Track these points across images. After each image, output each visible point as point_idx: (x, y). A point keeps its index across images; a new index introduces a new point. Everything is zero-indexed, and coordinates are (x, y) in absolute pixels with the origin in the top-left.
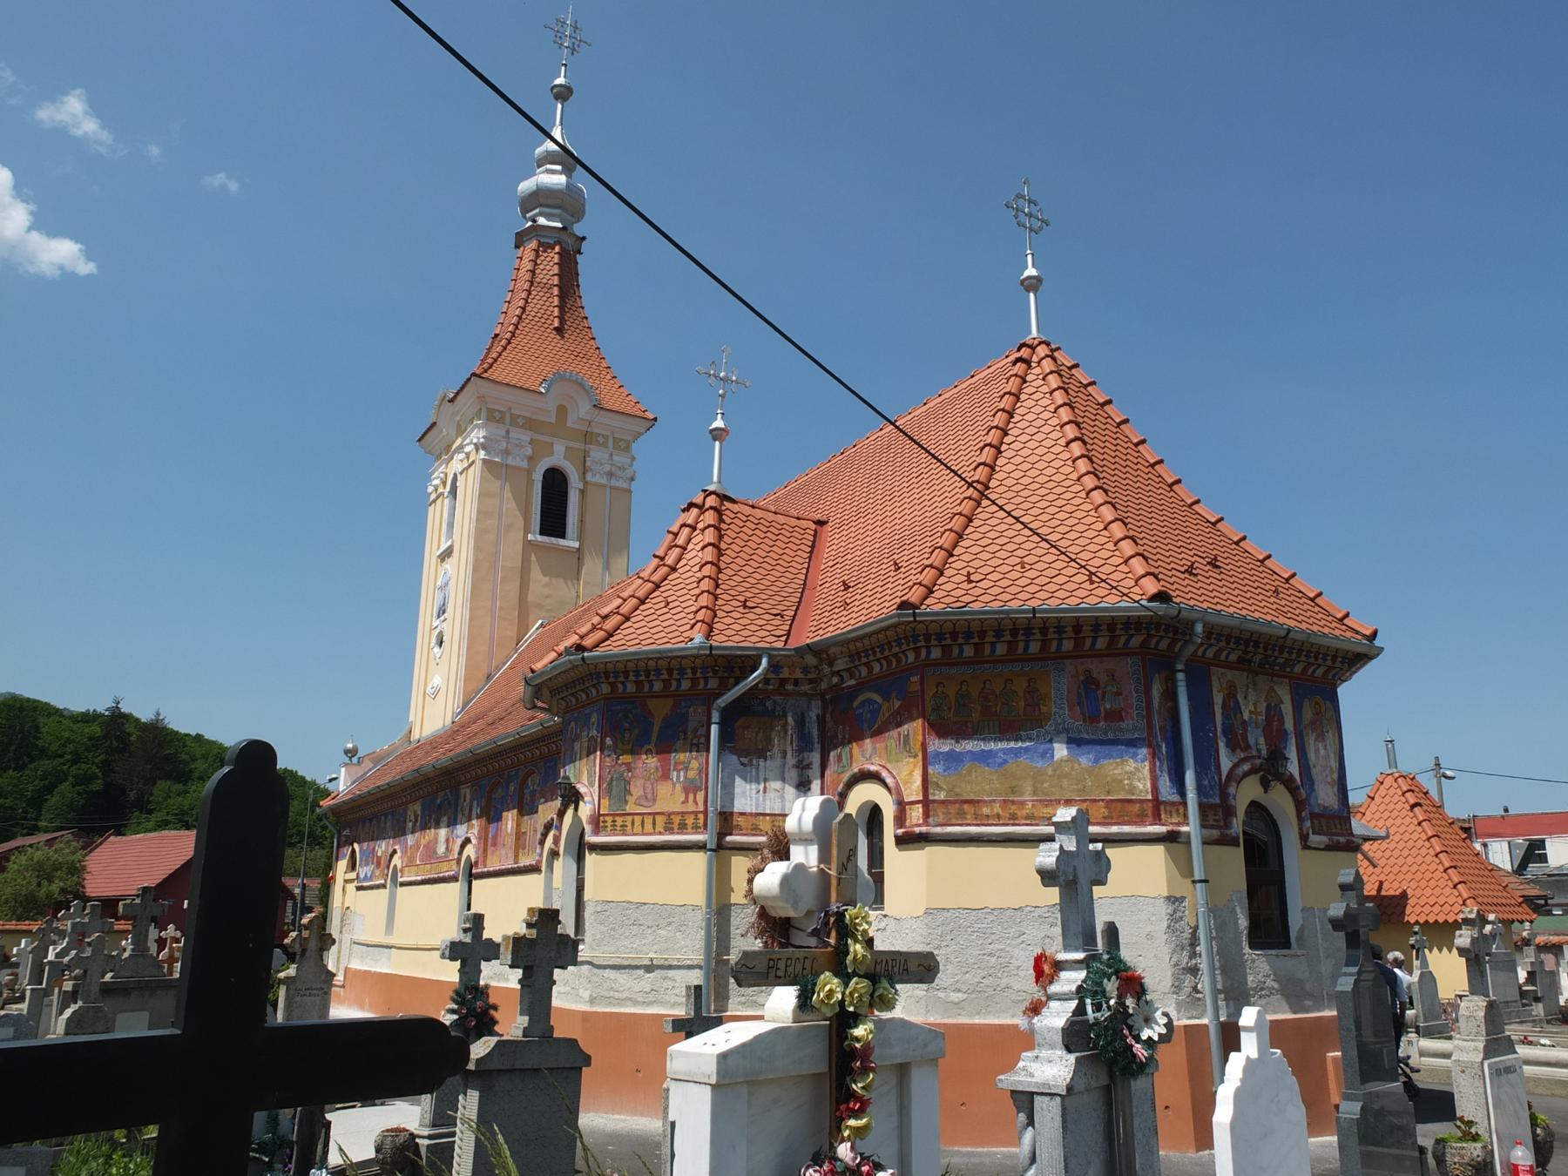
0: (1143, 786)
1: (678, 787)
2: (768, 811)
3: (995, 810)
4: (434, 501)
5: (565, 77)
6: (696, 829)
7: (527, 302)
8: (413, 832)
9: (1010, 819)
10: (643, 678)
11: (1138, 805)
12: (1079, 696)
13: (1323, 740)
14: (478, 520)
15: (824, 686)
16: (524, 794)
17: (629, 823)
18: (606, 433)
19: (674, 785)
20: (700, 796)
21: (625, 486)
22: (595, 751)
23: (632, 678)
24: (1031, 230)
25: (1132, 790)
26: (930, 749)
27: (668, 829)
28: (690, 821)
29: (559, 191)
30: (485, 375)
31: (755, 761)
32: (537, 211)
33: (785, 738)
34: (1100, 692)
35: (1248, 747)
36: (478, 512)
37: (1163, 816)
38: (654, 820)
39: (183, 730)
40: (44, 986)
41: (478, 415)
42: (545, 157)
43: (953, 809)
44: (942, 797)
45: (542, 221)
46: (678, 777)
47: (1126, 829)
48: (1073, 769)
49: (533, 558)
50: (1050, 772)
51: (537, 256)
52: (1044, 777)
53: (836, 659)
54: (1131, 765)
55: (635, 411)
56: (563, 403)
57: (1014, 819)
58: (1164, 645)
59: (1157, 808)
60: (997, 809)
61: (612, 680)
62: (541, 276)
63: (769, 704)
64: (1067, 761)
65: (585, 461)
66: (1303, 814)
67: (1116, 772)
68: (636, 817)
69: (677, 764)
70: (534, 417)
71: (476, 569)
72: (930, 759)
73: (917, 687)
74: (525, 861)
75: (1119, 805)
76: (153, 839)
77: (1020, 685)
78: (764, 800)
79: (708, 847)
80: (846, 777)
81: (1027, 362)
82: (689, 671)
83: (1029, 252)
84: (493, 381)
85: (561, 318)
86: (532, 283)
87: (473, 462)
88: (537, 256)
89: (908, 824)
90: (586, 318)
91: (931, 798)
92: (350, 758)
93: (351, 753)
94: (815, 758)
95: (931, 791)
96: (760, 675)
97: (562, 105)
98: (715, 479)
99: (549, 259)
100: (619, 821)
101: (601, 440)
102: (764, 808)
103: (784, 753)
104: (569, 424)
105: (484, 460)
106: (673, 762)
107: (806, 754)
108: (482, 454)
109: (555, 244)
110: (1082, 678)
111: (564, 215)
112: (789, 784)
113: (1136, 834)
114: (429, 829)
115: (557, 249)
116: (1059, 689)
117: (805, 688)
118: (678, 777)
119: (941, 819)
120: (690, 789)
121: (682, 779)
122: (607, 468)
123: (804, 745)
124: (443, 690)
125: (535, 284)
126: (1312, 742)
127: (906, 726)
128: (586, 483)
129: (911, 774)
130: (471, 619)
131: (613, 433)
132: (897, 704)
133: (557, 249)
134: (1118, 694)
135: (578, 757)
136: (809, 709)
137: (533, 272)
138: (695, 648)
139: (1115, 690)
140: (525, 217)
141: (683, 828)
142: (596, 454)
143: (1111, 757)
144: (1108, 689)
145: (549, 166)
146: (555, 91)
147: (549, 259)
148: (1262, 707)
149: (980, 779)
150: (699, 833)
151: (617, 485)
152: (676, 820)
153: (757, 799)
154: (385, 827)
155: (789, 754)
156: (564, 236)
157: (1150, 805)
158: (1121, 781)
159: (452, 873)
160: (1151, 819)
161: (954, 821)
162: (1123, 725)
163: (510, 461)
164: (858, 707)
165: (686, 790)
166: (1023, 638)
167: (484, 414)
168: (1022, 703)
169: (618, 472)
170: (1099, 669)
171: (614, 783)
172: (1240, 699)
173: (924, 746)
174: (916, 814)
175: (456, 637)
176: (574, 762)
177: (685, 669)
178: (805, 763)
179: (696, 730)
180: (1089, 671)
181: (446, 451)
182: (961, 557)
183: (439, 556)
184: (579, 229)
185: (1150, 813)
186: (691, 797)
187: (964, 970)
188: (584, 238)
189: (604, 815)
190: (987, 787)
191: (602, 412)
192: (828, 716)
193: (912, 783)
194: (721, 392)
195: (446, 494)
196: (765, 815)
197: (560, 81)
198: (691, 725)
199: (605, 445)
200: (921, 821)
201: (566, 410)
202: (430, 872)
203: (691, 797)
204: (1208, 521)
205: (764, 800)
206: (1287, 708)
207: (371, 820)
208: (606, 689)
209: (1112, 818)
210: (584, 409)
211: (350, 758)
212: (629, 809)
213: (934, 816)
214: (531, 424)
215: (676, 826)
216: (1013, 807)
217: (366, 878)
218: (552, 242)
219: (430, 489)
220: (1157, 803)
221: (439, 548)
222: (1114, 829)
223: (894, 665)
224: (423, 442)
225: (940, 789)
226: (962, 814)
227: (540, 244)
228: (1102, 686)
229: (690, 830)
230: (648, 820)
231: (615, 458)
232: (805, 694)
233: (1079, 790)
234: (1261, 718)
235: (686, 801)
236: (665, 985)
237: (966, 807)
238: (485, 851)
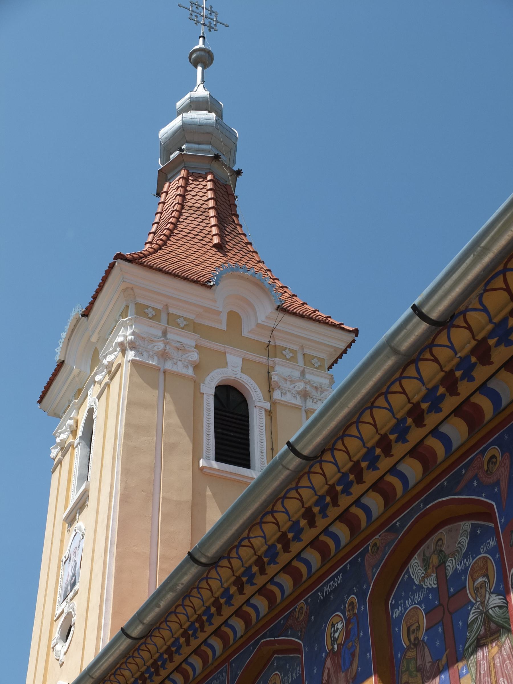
4: (60, 462)
14: (127, 435)
18: (295, 347)
36: (128, 424)
41: (124, 313)
49: (209, 492)
51: (187, 184)
71: (125, 499)
85: (221, 235)
97: (204, 68)
101: (289, 355)
104: (245, 333)
105: (133, 362)
108: (131, 355)
115: (209, 177)
122: (301, 386)
128: (274, 403)
130: (119, 570)
131: (302, 348)
137: (183, 196)
146: (194, 56)
147: (200, 187)
163: (169, 366)
167: (132, 309)
169: (314, 393)
183: (66, 519)
197: (200, 44)
199: (294, 359)
201: (239, 318)
231: (308, 377)
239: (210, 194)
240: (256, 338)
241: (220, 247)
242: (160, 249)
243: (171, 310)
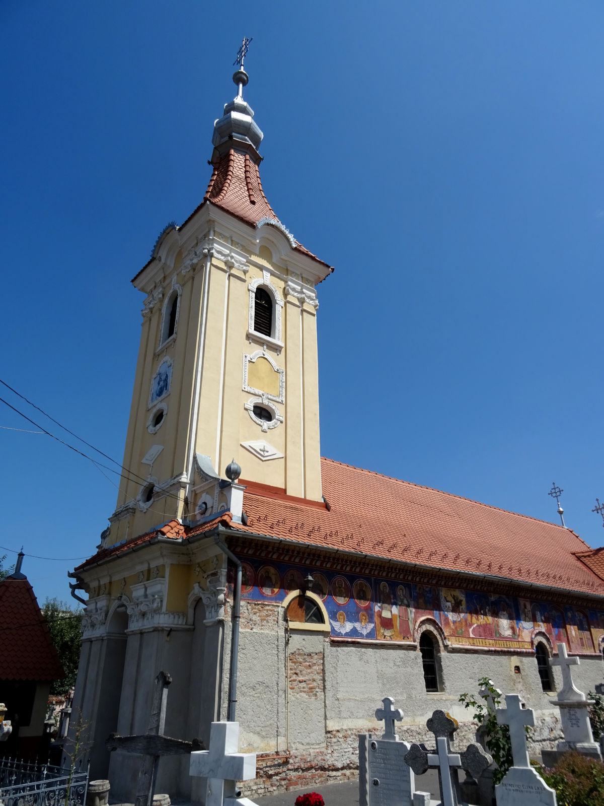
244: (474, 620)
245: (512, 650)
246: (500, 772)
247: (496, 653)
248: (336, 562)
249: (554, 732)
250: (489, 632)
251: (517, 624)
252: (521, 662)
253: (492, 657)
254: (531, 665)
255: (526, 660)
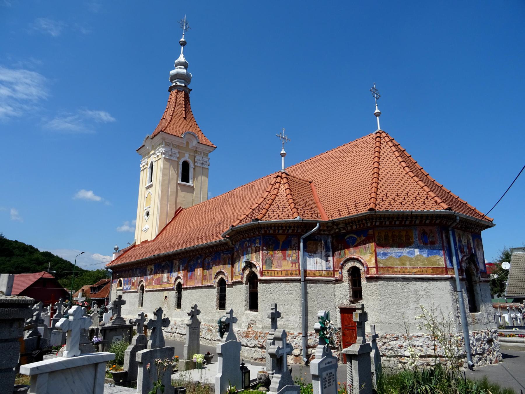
0: (442, 264)
1: (289, 262)
2: (318, 270)
3: (398, 270)
4: (143, 170)
5: (184, 38)
6: (296, 275)
7: (175, 109)
8: (150, 275)
9: (403, 272)
10: (277, 229)
11: (441, 269)
12: (422, 236)
13: (480, 251)
14: (163, 177)
15: (332, 232)
16: (204, 263)
17: (273, 273)
19: (288, 261)
20: (297, 265)
21: (207, 167)
22: (259, 251)
23: (273, 229)
24: (377, 98)
25: (439, 264)
26: (377, 252)
27: (287, 275)
28: (294, 273)
29: (184, 75)
30: (165, 131)
31: (313, 254)
32: (176, 80)
33: (321, 248)
34: (428, 236)
35: (464, 252)
36: (163, 174)
37: (448, 272)
38: (282, 272)
39: (10, 239)
40: (51, 327)
41: (161, 144)
42: (179, 64)
43: (385, 270)
44: (382, 266)
45: (178, 83)
46: (289, 259)
47: (439, 276)
48: (421, 258)
50: (414, 259)
51: (177, 94)
52: (412, 260)
53: (340, 224)
54: (438, 257)
55: (210, 144)
56: (188, 141)
57: (404, 273)
58: (444, 222)
59: (446, 270)
60: (399, 269)
61: (266, 229)
62: (179, 101)
63: (316, 237)
64: (419, 256)
65: (195, 159)
66: (478, 272)
67: (434, 259)
68: (275, 271)
69: (288, 255)
70: (179, 145)
72: (378, 254)
73: (372, 233)
74: (206, 284)
75: (435, 269)
76: (19, 276)
77: (404, 233)
78: (316, 266)
79: (301, 280)
80: (344, 260)
81: (380, 137)
82: (292, 227)
83: (376, 105)
84: (167, 133)
85: (186, 114)
86: (176, 103)
87: (160, 158)
88: (177, 94)
89: (370, 273)
90: (193, 115)
91: (378, 266)
92: (116, 251)
93: (116, 249)
94: (331, 253)
95: (378, 264)
96: (317, 229)
98: (283, 168)
99: (181, 96)
100: (270, 272)
102: (317, 269)
103: (322, 252)
104: (190, 148)
105: (164, 158)
106: (287, 255)
107: (328, 252)
108: (164, 156)
109: (183, 91)
110: (422, 231)
111: (185, 82)
112: (324, 260)
113: (442, 277)
114: (159, 273)
115: (183, 92)
116: (415, 235)
117: (327, 232)
118: (289, 259)
119: (382, 272)
120: (294, 263)
121: (290, 259)
122: (201, 162)
123: (327, 250)
124: (150, 229)
125: (177, 103)
126: (477, 251)
127: (368, 245)
128: (195, 166)
129: (370, 259)
131: (203, 151)
132: (363, 238)
133: (183, 92)
134: (433, 236)
135: (250, 252)
136: (328, 239)
137: (176, 99)
138: (297, 220)
139: (432, 235)
140: (172, 82)
141: (292, 274)
142: (198, 157)
143: (432, 255)
144: (430, 235)
145: (180, 66)
147: (181, 96)
148: (466, 241)
149: (393, 261)
150: (297, 276)
151: (205, 167)
152: (289, 272)
153: (314, 266)
154: (136, 273)
155: (323, 252)
156: (185, 88)
157: (445, 269)
158: (436, 262)
159: (171, 288)
160: (445, 273)
161: (386, 273)
162: (435, 246)
163: (172, 158)
164: (347, 239)
165: (292, 263)
166: (414, 219)
167: (164, 143)
168: (404, 239)
170: (427, 229)
171: (267, 261)
172: (461, 238)
173: (375, 251)
174: (373, 271)
175: (156, 212)
176: (249, 254)
177: (291, 226)
178: (328, 255)
179: (294, 245)
180: (424, 230)
181: (147, 154)
182: (380, 195)
184: (189, 87)
185: (445, 271)
186: (294, 265)
187: (392, 317)
188: (191, 90)
189: (264, 271)
190: (395, 263)
191: (201, 145)
192: (334, 241)
193: (371, 262)
194: (283, 142)
195: (148, 168)
196: (317, 270)
197: (182, 39)
198: (293, 243)
200: (375, 273)
202: (160, 287)
203: (294, 265)
204: (439, 186)
205: (316, 266)
206: (471, 241)
207: (129, 271)
208: (263, 232)
209: (433, 272)
210: (195, 143)
211: (116, 251)
212: (273, 269)
213: (380, 271)
214: (178, 147)
215: (289, 274)
216: (404, 269)
217: (127, 289)
218: (181, 90)
219: (141, 166)
220: (446, 268)
221: (146, 185)
222: (435, 276)
223: (362, 227)
224: (138, 151)
225: (381, 263)
226: (388, 271)
227: (178, 91)
228: (428, 234)
229: (294, 275)
230: (276, 272)
232: (326, 234)
233: (423, 264)
234: (466, 244)
235: (292, 266)
236: (288, 323)
237: (389, 269)
238: (187, 280)
239: (183, 98)
240: (192, 149)
241: (185, 118)
242: (170, 121)
243: (173, 143)
244: (155, 277)
245: (166, 288)
246: (84, 293)
247: (156, 291)
248: (280, 229)
249: (173, 329)
250: (159, 281)
251: (170, 274)
252: (168, 294)
253: (158, 293)
254: (173, 295)
255: (171, 293)
